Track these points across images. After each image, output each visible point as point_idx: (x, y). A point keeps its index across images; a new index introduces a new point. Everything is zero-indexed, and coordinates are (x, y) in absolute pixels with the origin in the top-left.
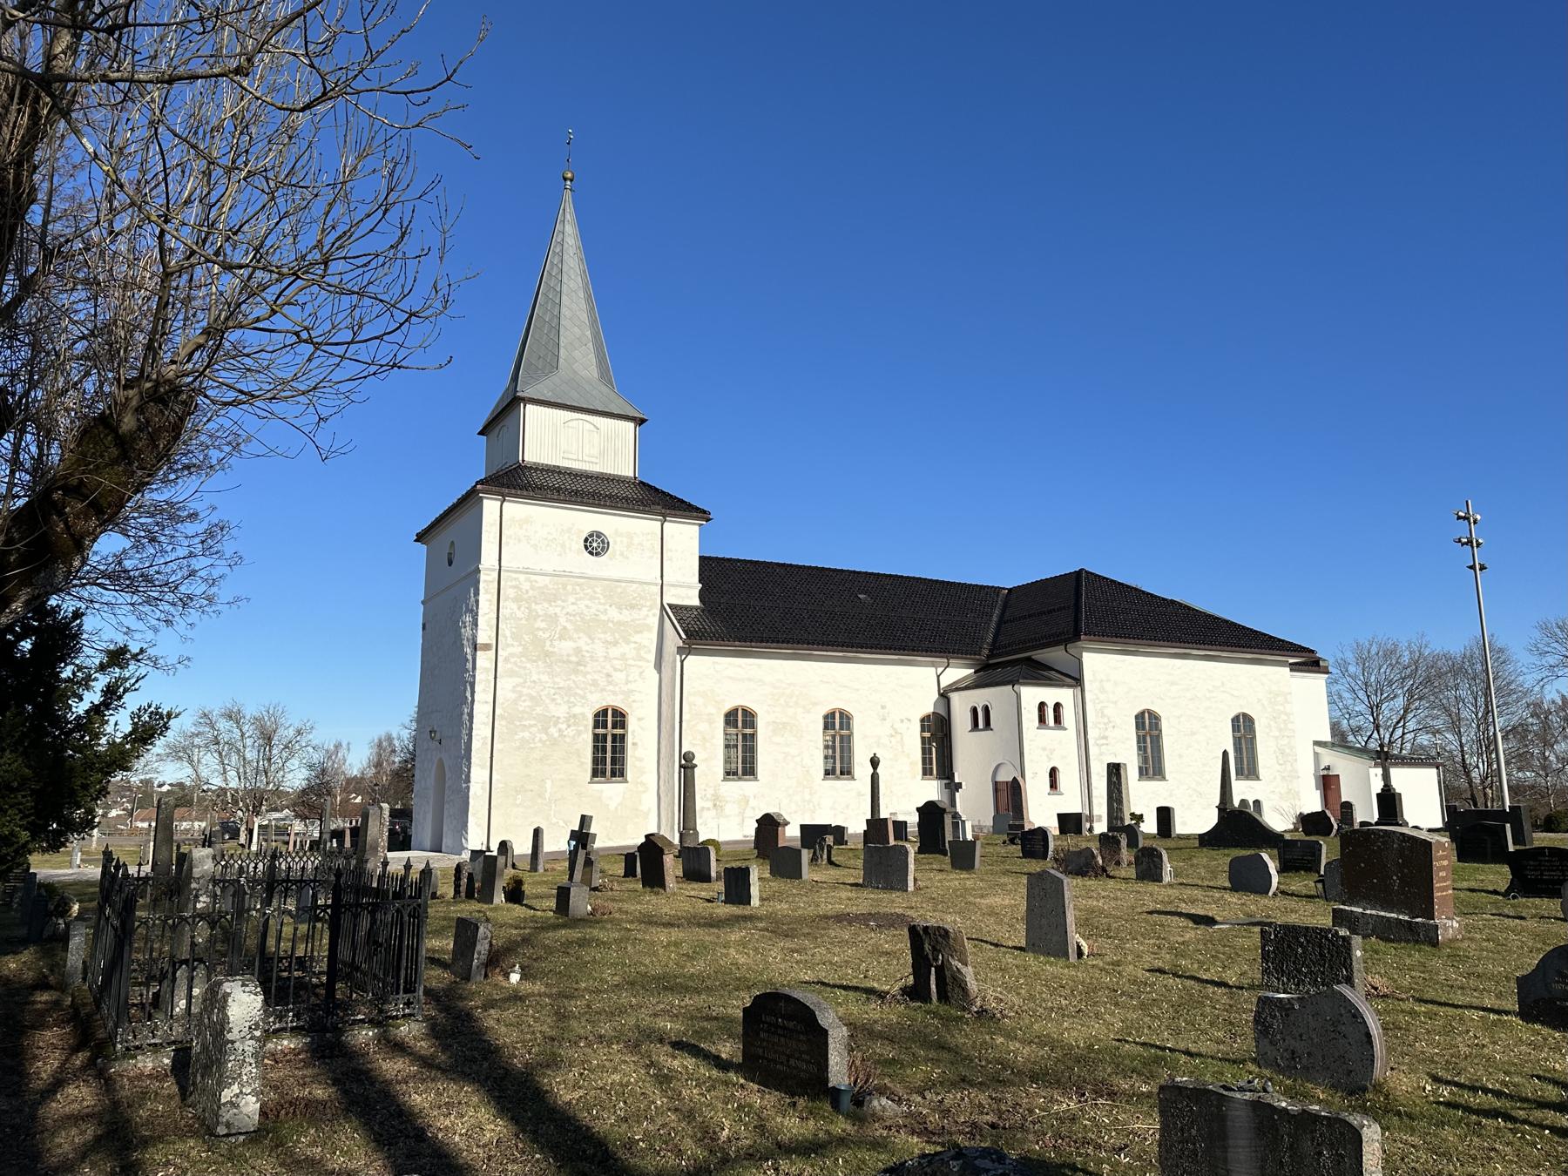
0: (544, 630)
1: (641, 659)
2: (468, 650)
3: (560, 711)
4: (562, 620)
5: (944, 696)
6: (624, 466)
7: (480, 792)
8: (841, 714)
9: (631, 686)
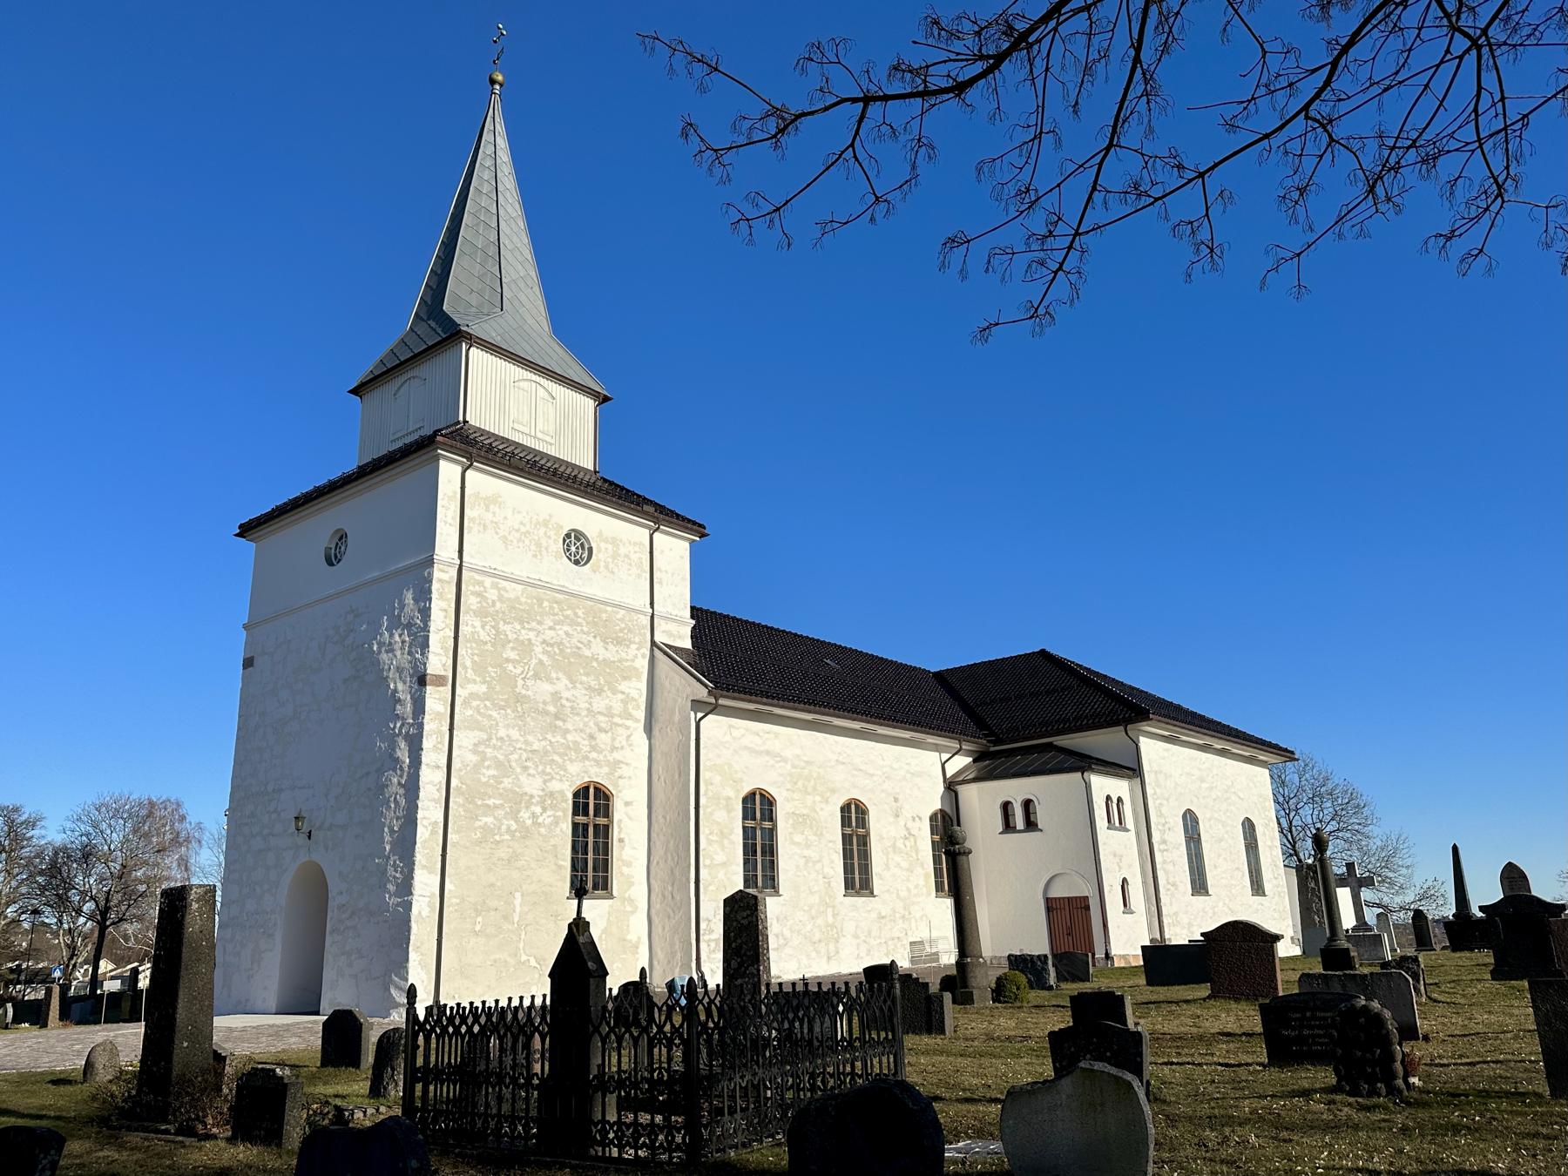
0: (513, 661)
1: (629, 716)
2: (402, 689)
3: (532, 785)
4: (538, 649)
5: (951, 786)
6: (583, 456)
7: (426, 912)
8: (857, 806)
9: (617, 755)
